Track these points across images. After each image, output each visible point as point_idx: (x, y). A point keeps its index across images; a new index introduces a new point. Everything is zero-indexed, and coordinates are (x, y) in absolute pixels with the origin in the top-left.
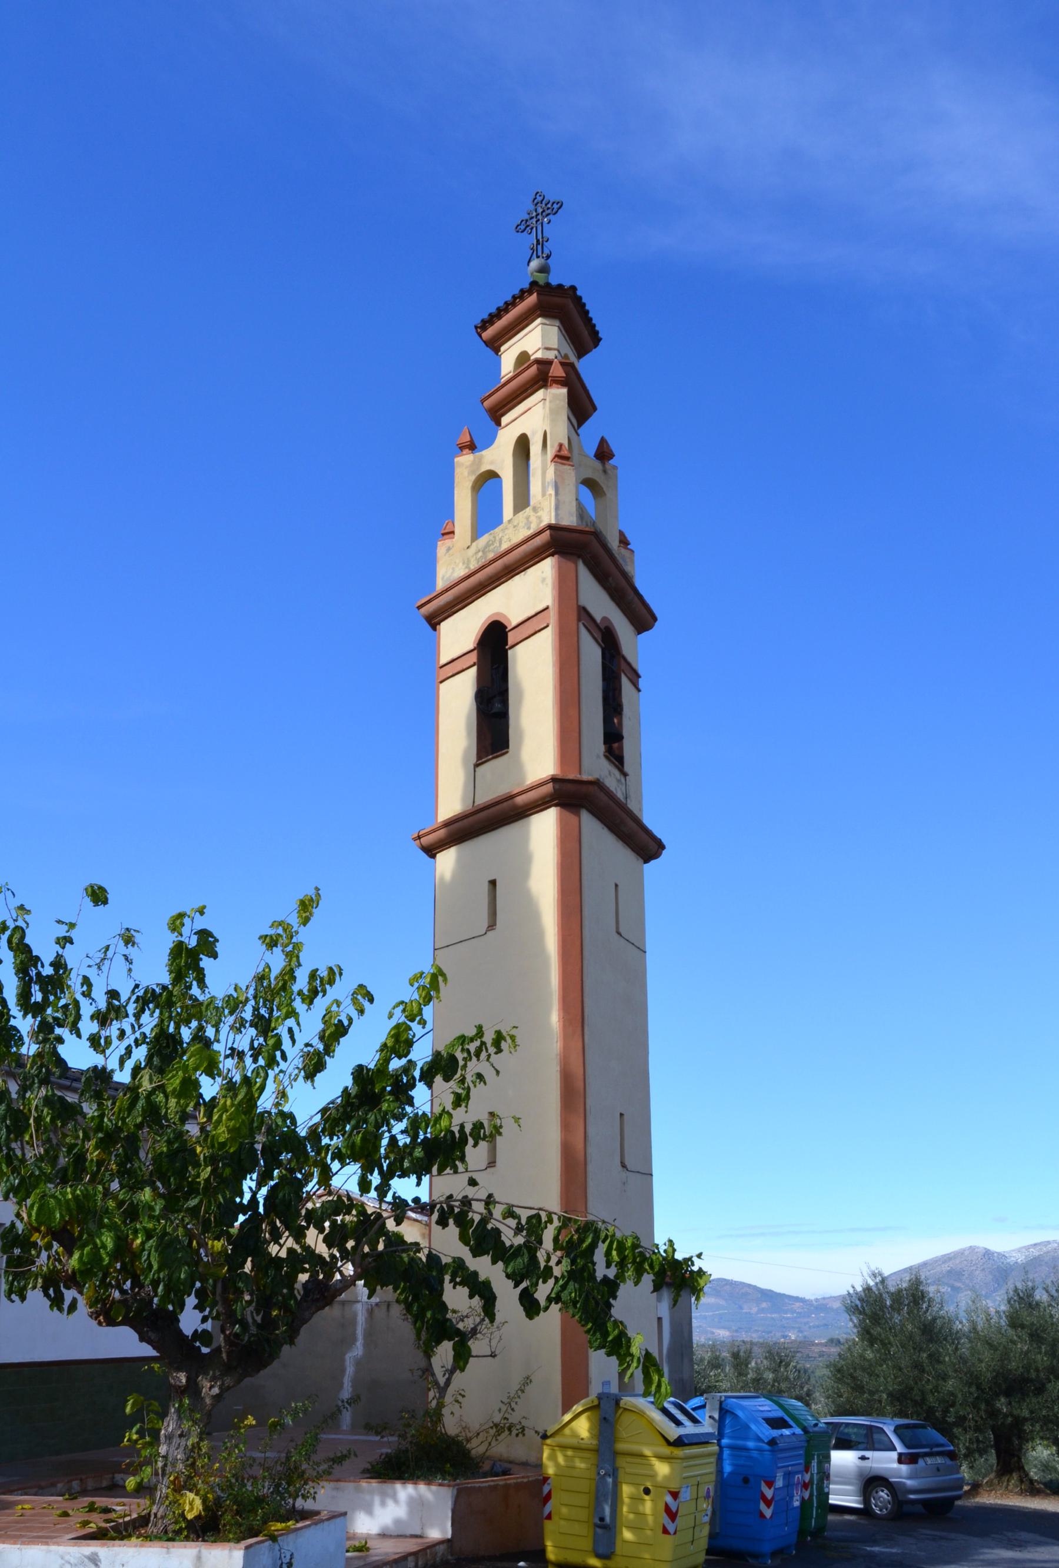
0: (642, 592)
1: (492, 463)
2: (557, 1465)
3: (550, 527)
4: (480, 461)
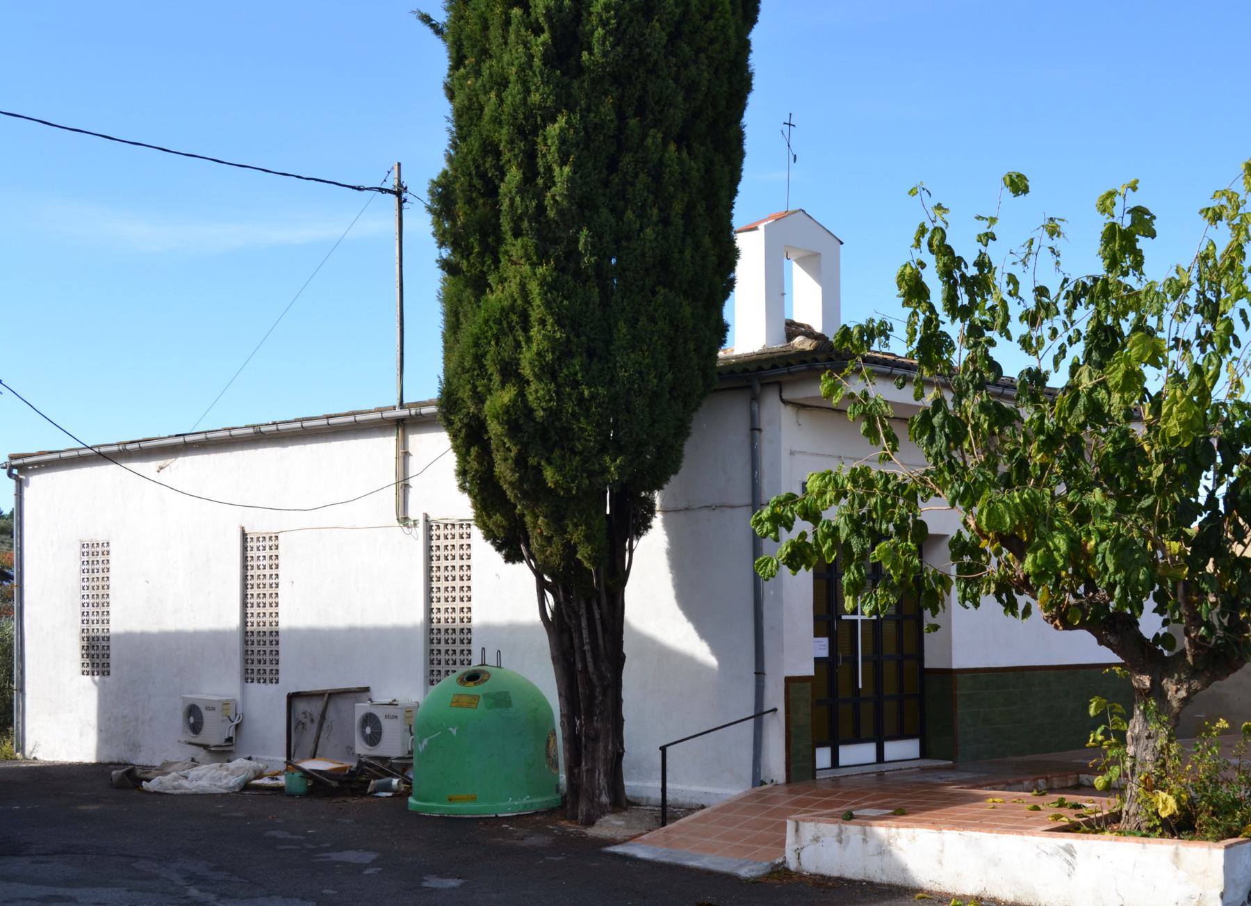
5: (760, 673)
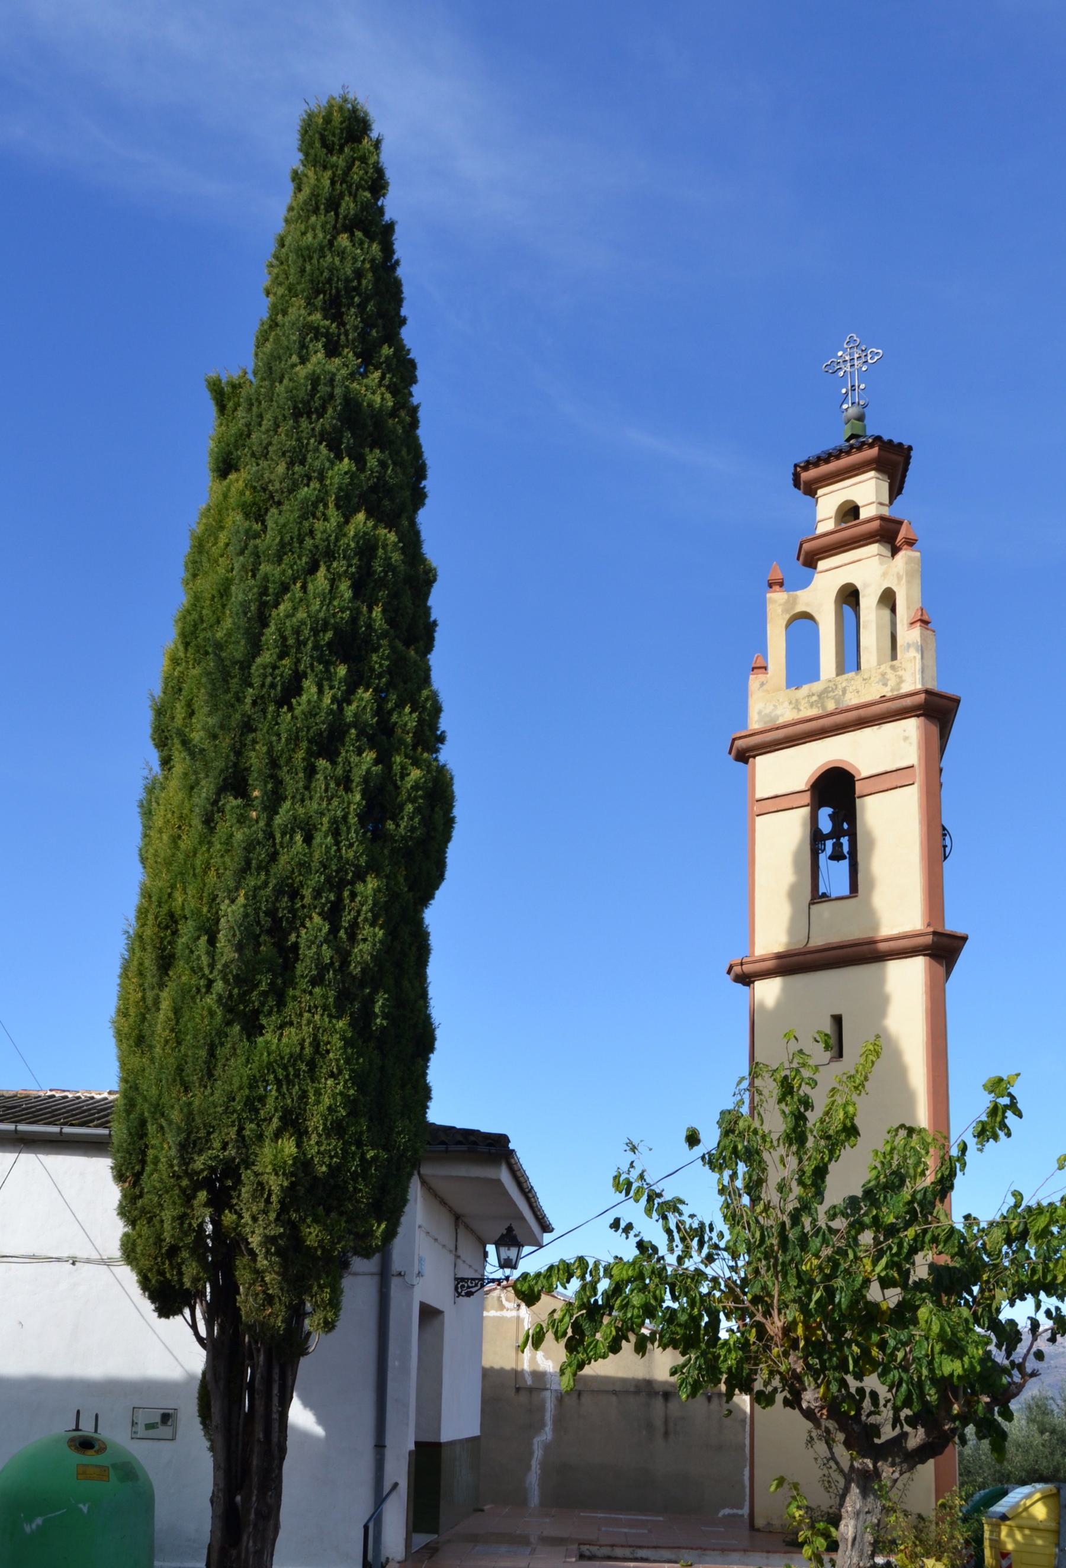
0: (867, 731)
1: (807, 605)
2: (1016, 1542)
3: (928, 692)
4: (794, 601)
5: (380, 1446)
